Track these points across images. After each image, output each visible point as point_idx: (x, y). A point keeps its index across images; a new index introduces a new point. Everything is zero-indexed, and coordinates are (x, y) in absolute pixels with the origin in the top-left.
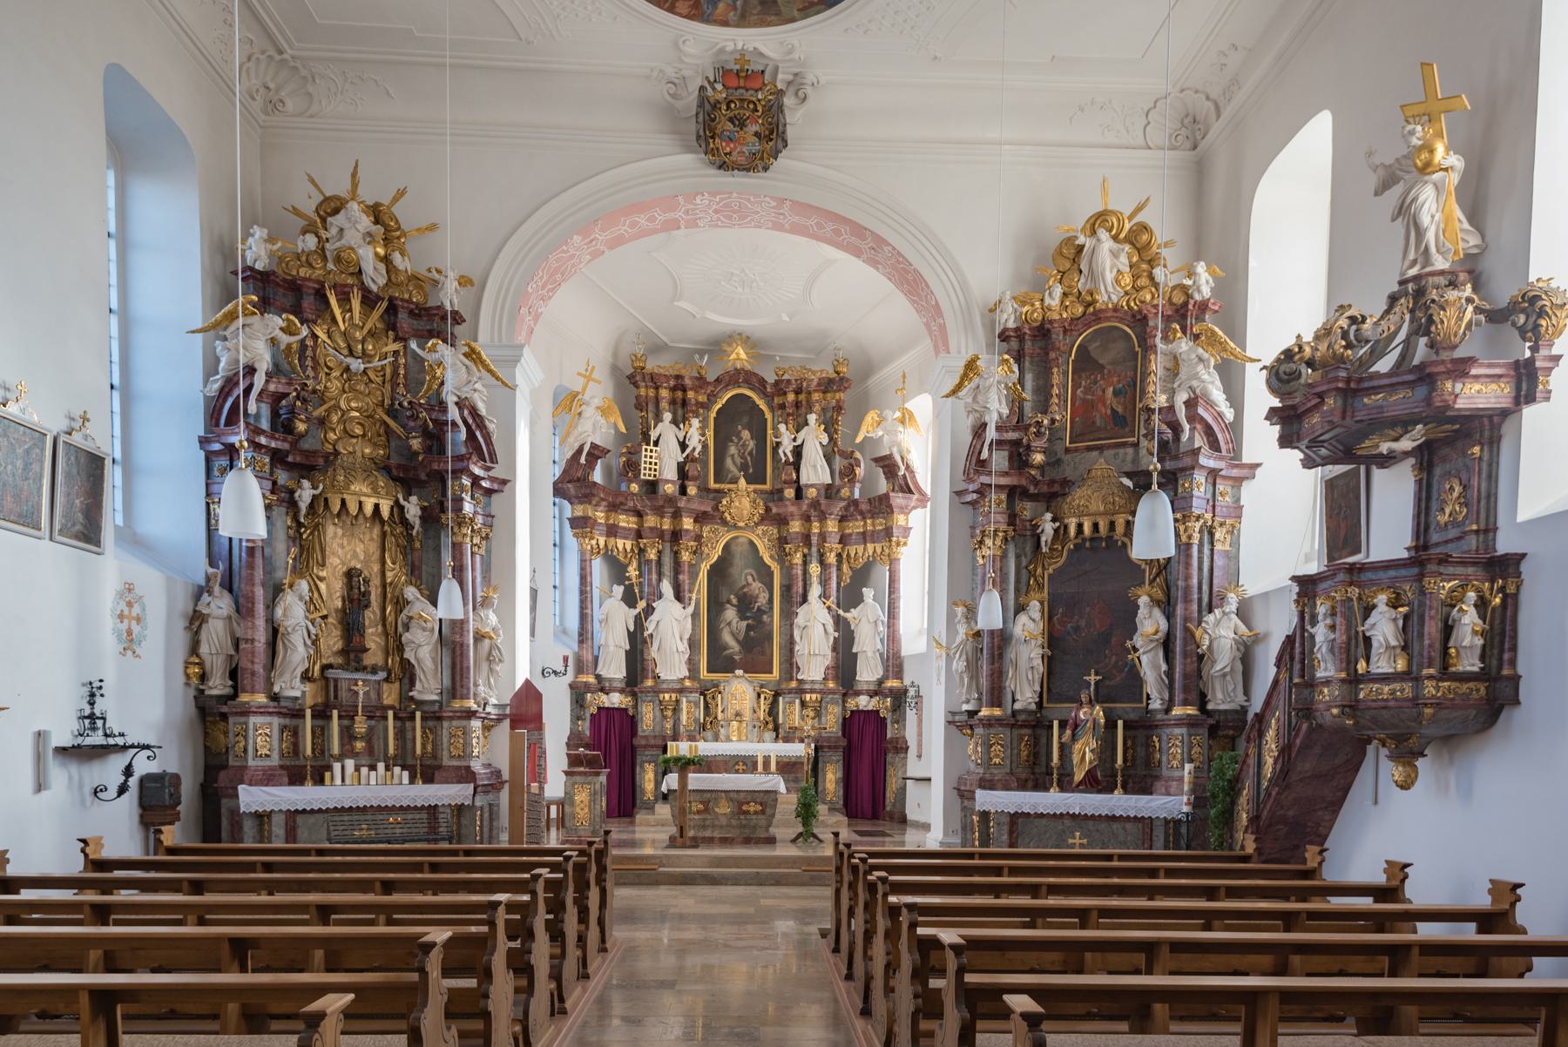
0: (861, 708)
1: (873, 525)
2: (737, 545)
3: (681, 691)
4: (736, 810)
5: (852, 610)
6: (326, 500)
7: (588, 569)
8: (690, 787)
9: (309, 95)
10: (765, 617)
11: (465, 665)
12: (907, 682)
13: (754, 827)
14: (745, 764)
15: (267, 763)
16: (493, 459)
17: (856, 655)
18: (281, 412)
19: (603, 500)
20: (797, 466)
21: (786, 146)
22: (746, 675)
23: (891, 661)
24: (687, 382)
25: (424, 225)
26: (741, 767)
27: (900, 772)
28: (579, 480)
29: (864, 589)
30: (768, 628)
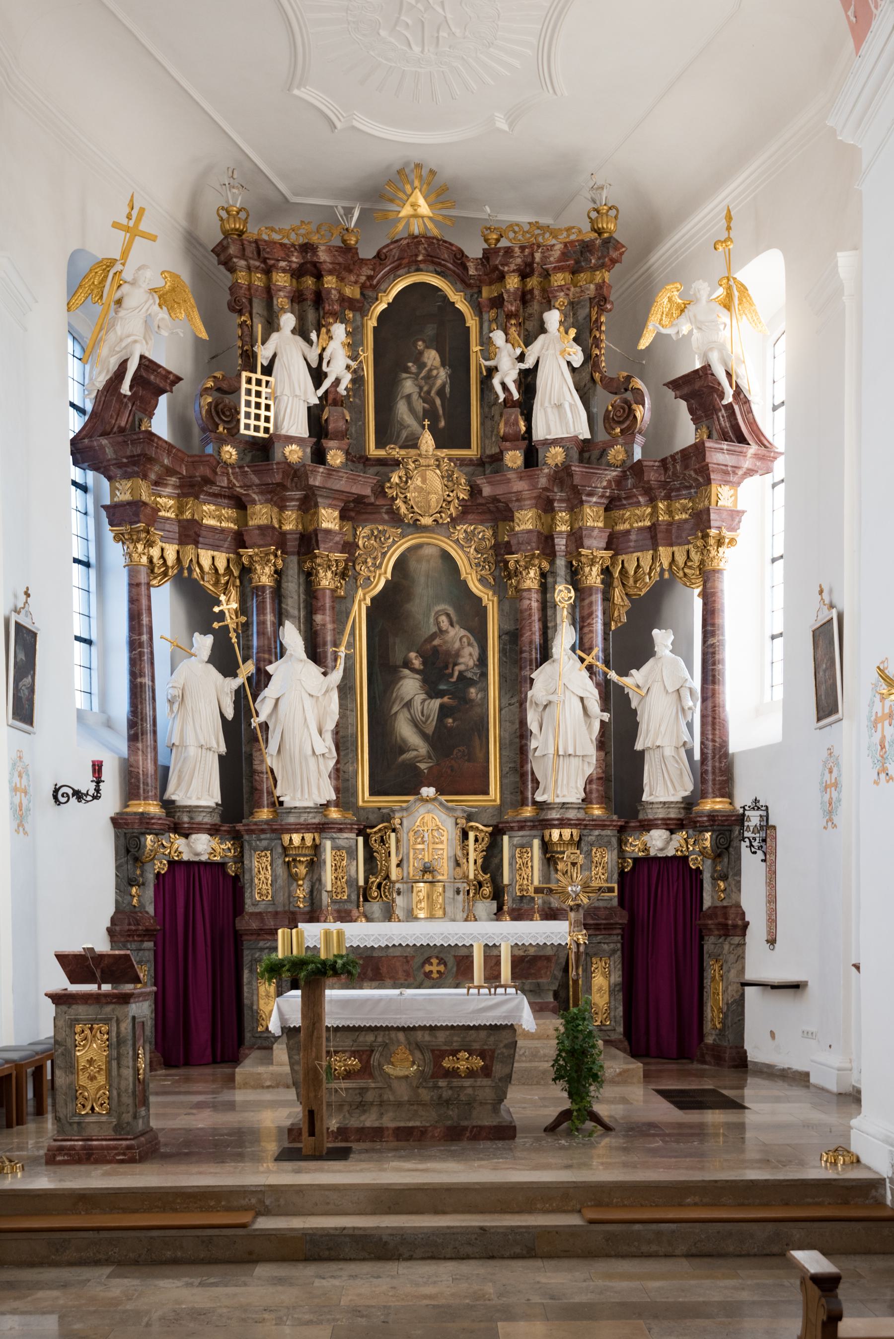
0: (653, 853)
1: (670, 512)
2: (419, 561)
3: (322, 828)
4: (429, 1070)
5: (634, 672)
7: (144, 602)
8: (330, 1021)
10: (473, 690)
12: (742, 798)
13: (470, 1104)
14: (442, 961)
17: (642, 753)
19: (170, 472)
22: (443, 798)
23: (710, 763)
24: (323, 256)
26: (434, 968)
27: (732, 974)
28: (122, 430)
29: (655, 632)
30: (478, 710)
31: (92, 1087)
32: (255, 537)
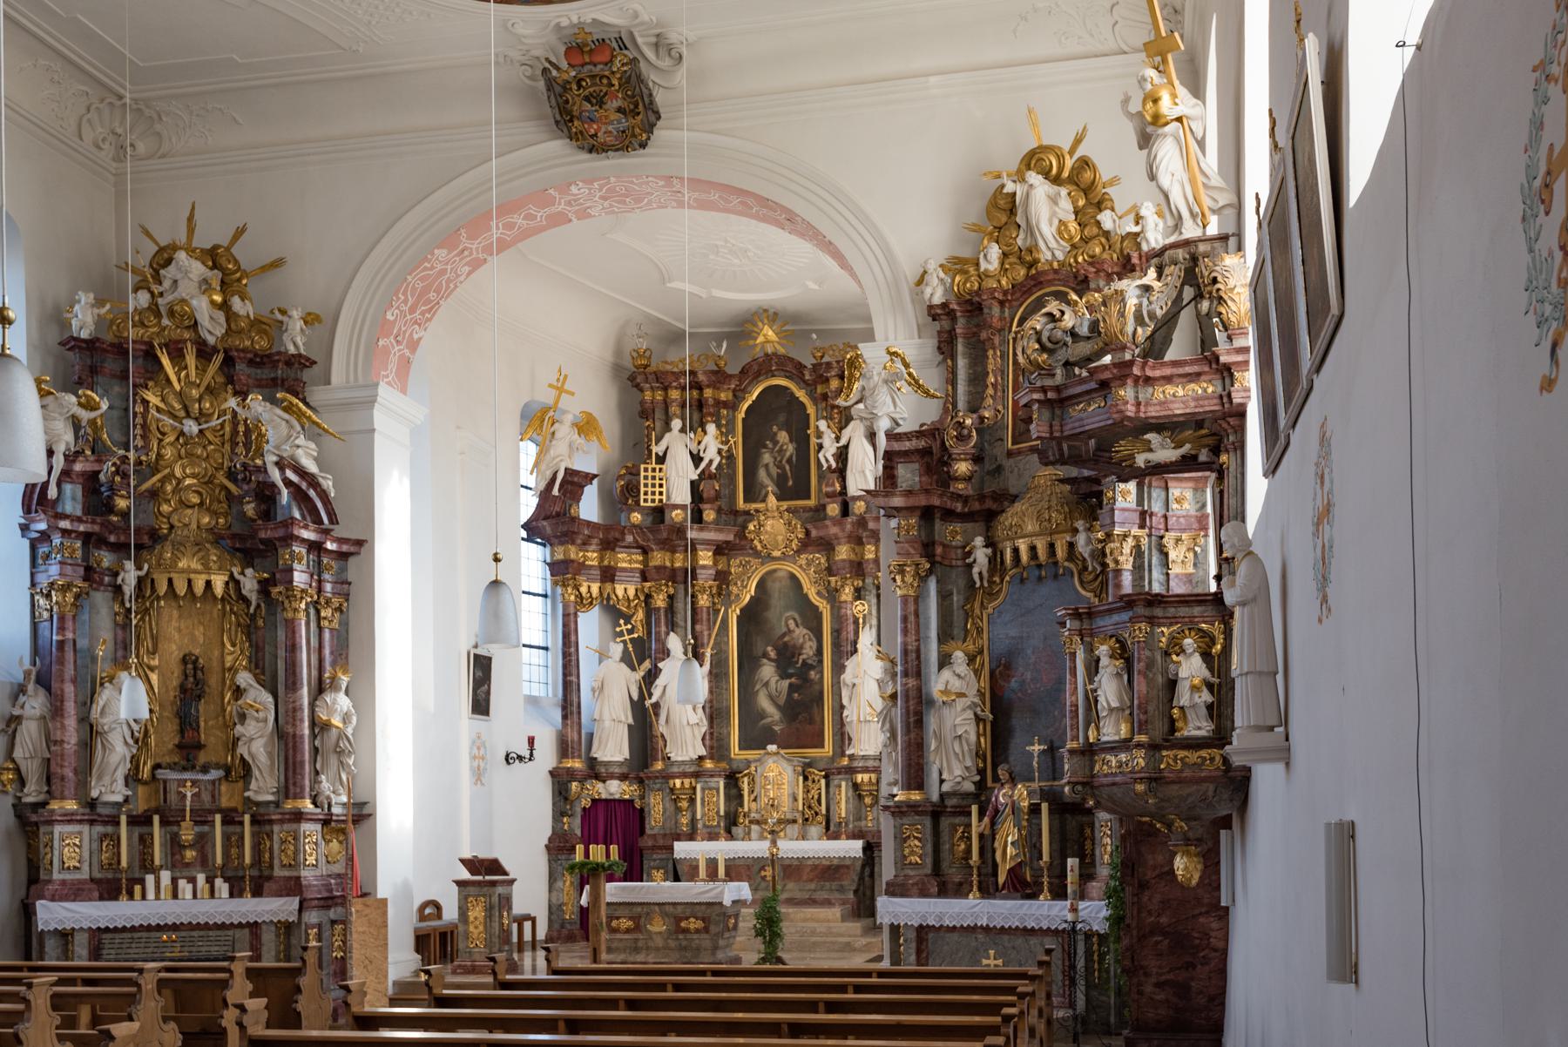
2: (773, 581)
4: (673, 928)
6: (153, 581)
9: (159, 134)
10: (812, 673)
11: (298, 759)
13: (698, 949)
15: (77, 876)
16: (333, 519)
18: (103, 489)
20: (841, 472)
21: (659, 118)
22: (782, 752)
24: (701, 377)
25: (269, 261)
28: (558, 514)
31: (476, 932)
32: (653, 574)
